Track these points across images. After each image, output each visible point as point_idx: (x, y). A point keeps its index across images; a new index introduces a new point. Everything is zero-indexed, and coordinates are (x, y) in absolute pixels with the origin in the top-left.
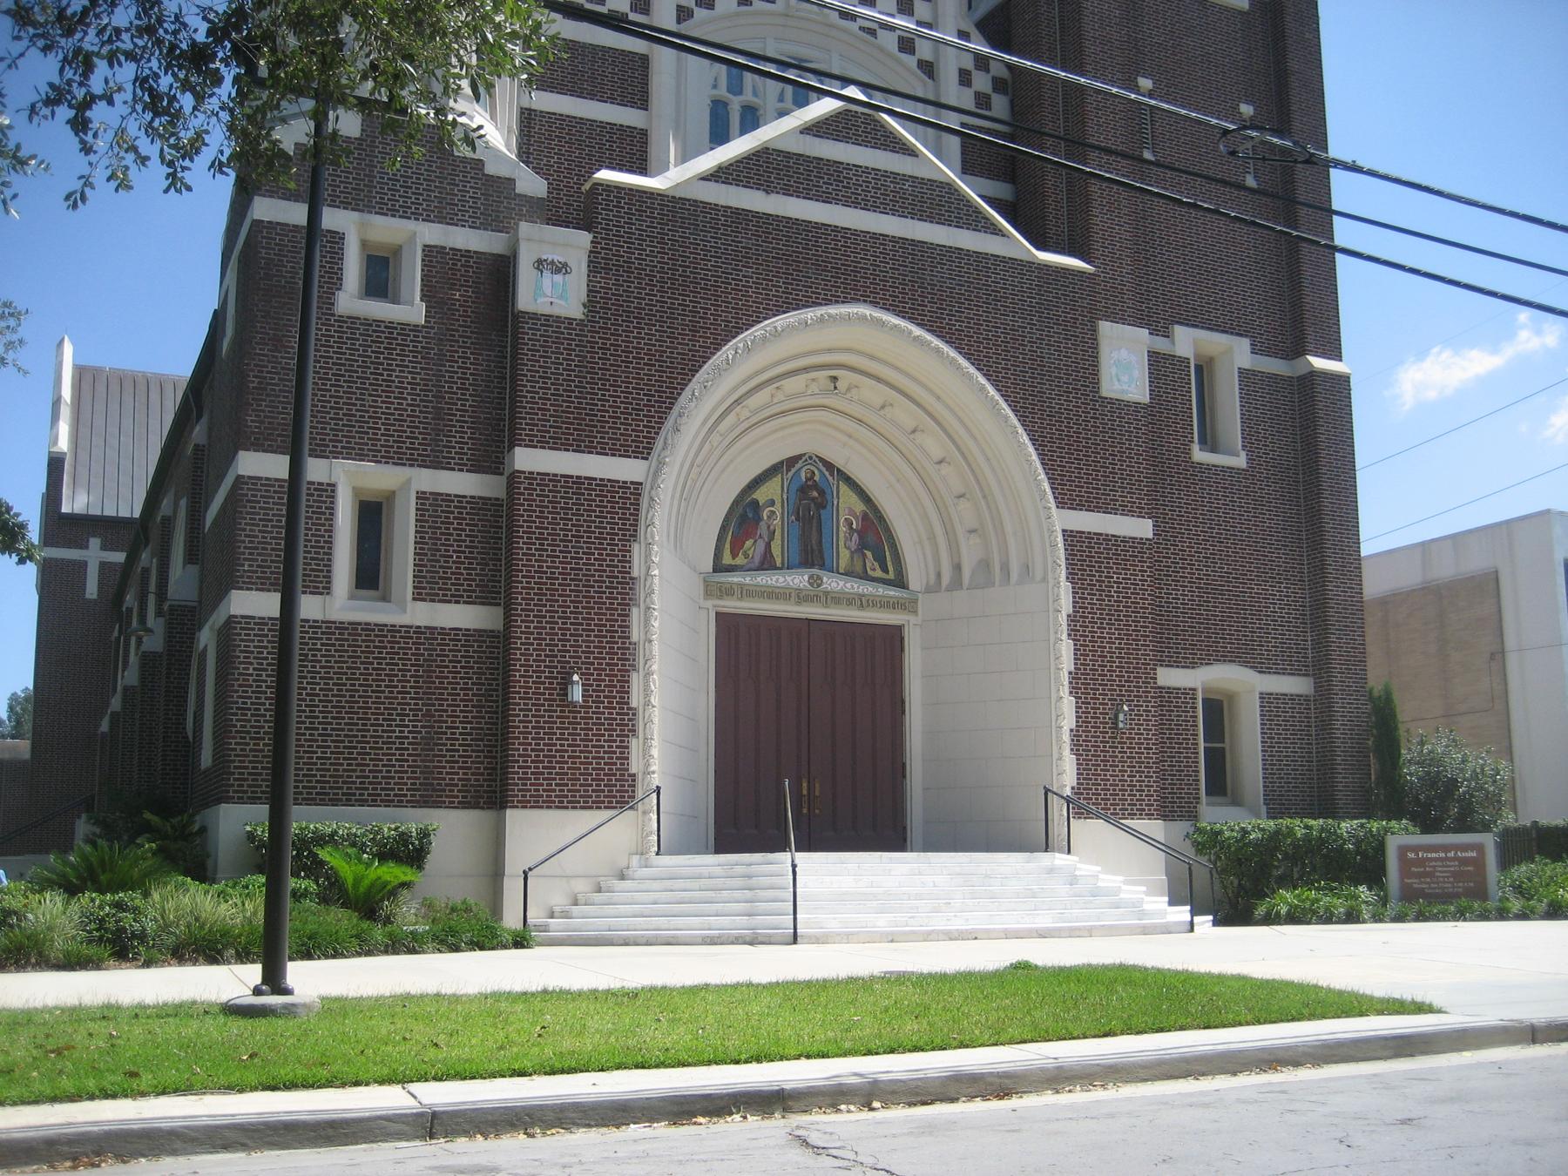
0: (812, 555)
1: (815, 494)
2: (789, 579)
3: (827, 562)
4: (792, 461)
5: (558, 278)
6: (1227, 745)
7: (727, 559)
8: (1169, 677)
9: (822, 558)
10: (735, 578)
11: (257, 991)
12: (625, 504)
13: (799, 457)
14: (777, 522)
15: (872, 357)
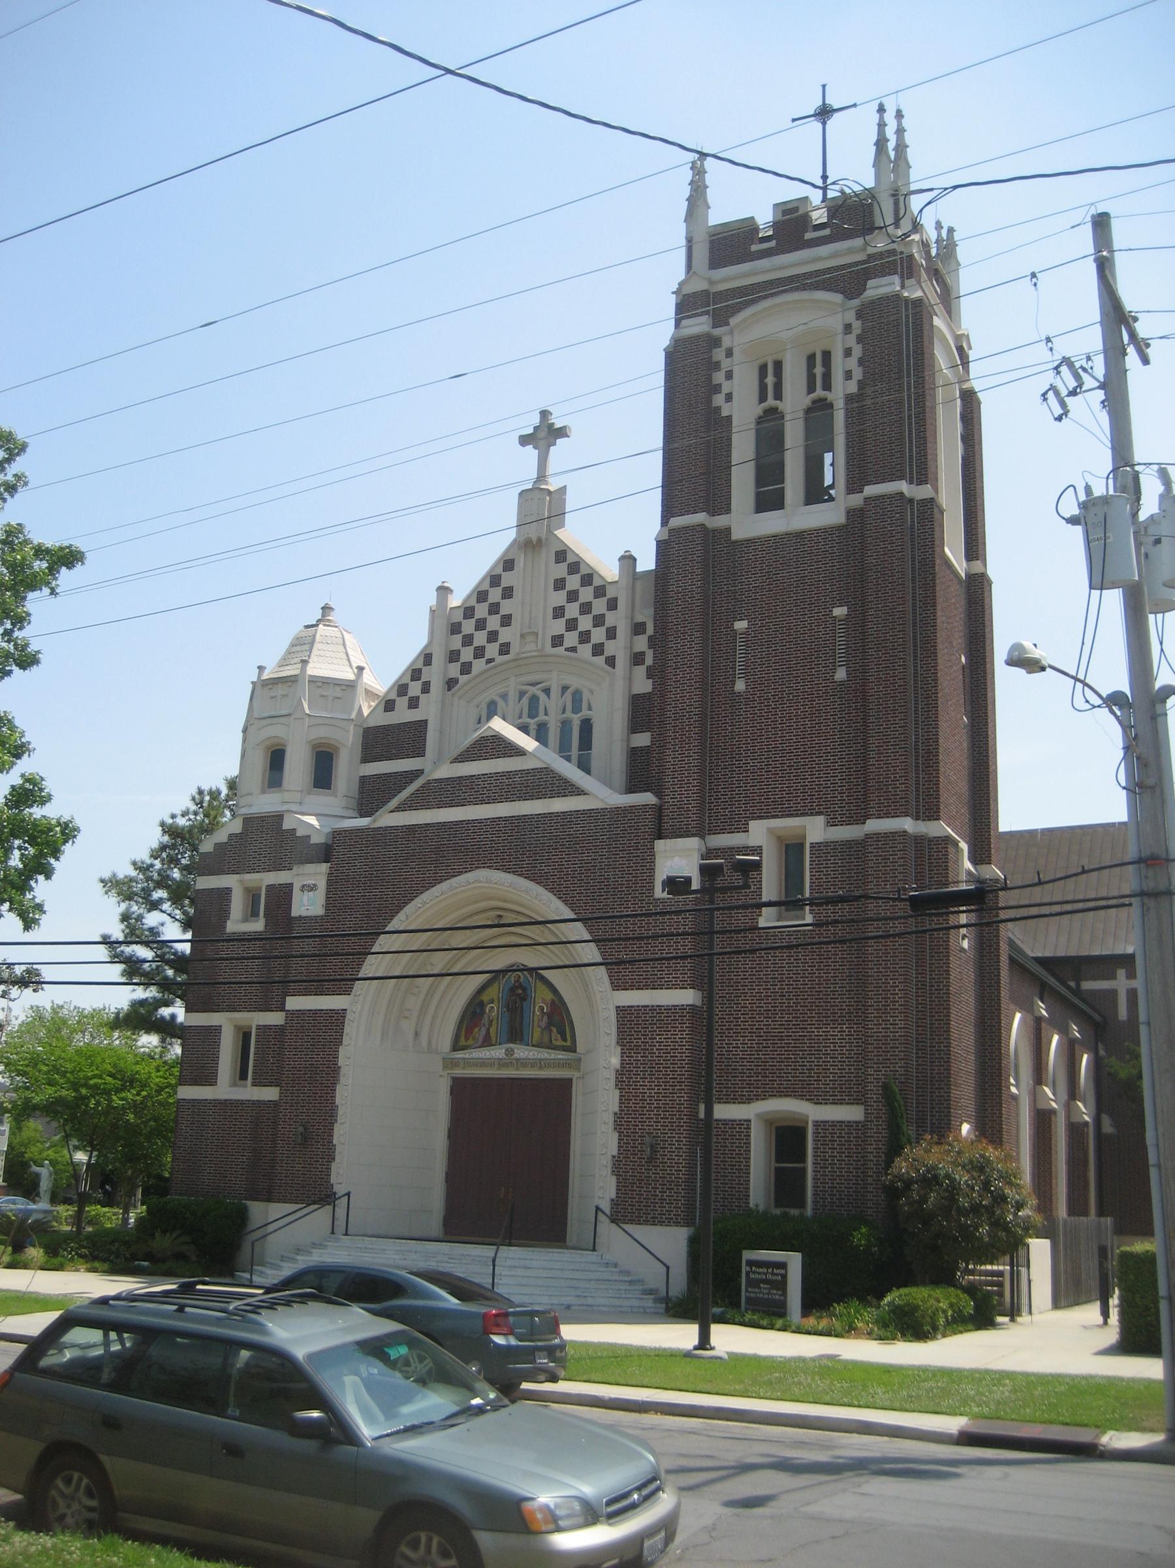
0: (516, 1034)
3: (525, 1037)
6: (774, 1165)
7: (463, 1042)
11: (696, 1348)
15: (505, 901)
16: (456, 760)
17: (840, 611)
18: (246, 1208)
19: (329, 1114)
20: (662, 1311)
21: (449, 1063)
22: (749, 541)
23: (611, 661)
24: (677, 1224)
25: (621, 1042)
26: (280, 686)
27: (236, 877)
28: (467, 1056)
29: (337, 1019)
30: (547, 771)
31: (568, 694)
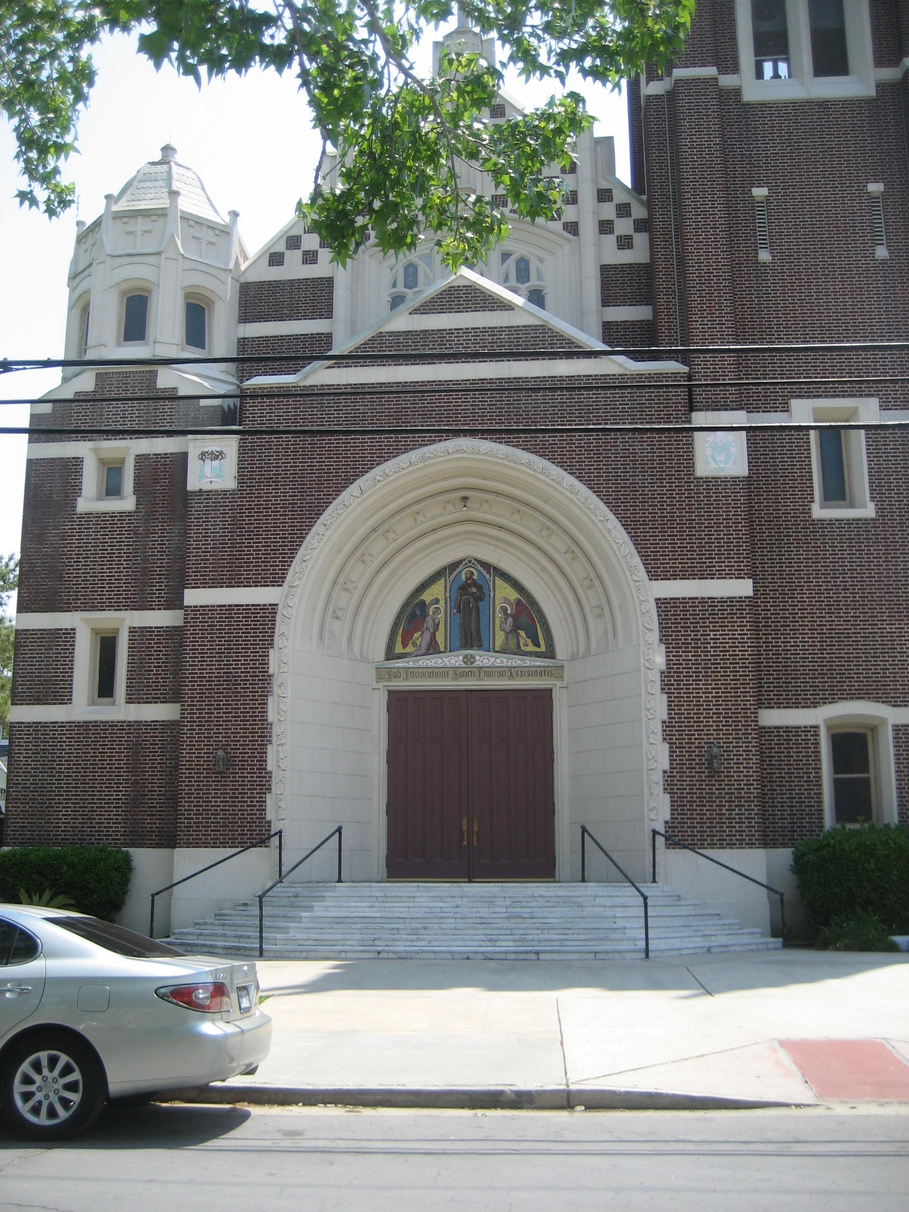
0: (471, 637)
1: (474, 590)
3: (485, 644)
4: (453, 566)
5: (216, 463)
6: (871, 775)
7: (399, 649)
8: (772, 717)
9: (480, 640)
10: (400, 663)
14: (441, 616)
15: (484, 478)
16: (415, 311)
17: (875, 188)
18: (127, 859)
19: (259, 734)
20: (780, 945)
21: (382, 674)
22: (763, 105)
23: (573, 228)
24: (751, 845)
25: (665, 638)
26: (140, 219)
27: (90, 444)
28: (411, 664)
29: (265, 616)
30: (544, 330)
31: (511, 261)
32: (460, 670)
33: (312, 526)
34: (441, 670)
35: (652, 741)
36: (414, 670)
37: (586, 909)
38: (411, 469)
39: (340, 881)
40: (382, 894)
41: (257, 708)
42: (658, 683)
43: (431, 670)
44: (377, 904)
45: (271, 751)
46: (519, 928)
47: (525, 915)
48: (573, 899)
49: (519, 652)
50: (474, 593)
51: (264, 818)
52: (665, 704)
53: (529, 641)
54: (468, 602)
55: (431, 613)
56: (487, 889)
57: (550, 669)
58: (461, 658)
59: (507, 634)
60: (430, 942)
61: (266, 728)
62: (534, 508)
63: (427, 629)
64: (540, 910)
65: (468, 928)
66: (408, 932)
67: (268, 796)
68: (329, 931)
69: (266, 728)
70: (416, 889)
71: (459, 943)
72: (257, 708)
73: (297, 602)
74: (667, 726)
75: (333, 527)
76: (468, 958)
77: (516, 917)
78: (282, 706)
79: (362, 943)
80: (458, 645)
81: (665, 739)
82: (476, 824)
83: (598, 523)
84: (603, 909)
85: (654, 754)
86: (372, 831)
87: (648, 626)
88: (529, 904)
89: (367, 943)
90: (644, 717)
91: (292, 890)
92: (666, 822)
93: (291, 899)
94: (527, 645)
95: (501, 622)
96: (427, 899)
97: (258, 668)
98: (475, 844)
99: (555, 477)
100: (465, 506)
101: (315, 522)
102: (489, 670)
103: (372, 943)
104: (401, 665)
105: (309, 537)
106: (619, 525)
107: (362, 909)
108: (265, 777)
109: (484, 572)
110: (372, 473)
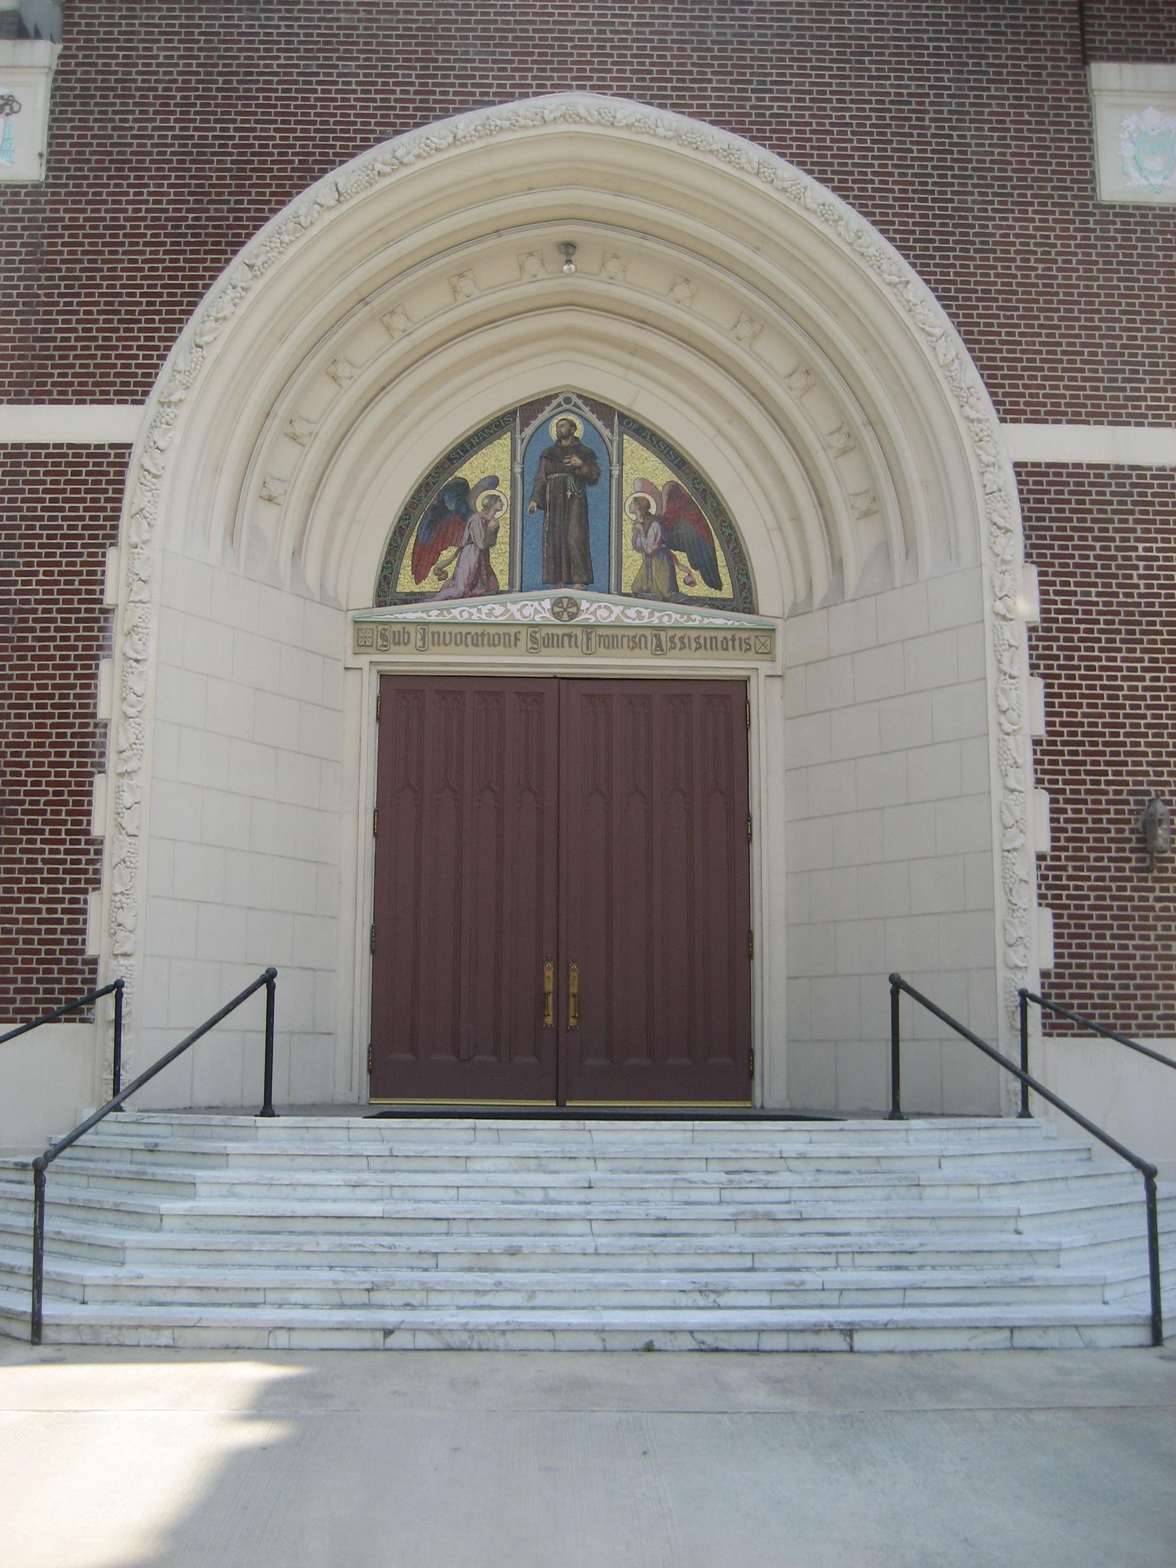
0: (569, 561)
1: (576, 461)
2: (513, 608)
4: (531, 409)
7: (406, 583)
10: (410, 613)
12: (92, 485)
13: (545, 401)
14: (502, 516)
21: (369, 637)
25: (1035, 552)
28: (434, 616)
32: (545, 631)
33: (221, 269)
34: (501, 630)
35: (1012, 784)
36: (442, 629)
37: (928, 1192)
38: (454, 152)
39: (267, 1110)
40: (382, 1149)
41: (73, 687)
42: (1024, 652)
43: (479, 630)
44: (366, 1177)
45: (102, 789)
46: (773, 1252)
47: (780, 1211)
48: (885, 1165)
49: (673, 595)
50: (575, 468)
51: (82, 952)
52: (1040, 700)
53: (696, 575)
54: (564, 486)
55: (479, 508)
56: (652, 1137)
57: (744, 635)
58: (547, 604)
59: (648, 557)
60: (532, 1294)
61: (93, 735)
62: (727, 264)
63: (470, 541)
64: (808, 1194)
65: (634, 1251)
66: (464, 1261)
67: (92, 897)
68: (240, 1258)
69: (93, 735)
70: (469, 1135)
71: (617, 1298)
72: (73, 687)
73: (177, 440)
74: (1047, 756)
75: (270, 273)
76: (649, 1348)
77: (756, 1217)
78: (131, 680)
79: (334, 1298)
80: (539, 579)
81: (1039, 781)
82: (574, 975)
83: (887, 292)
84: (971, 1192)
85: (1018, 814)
86: (336, 997)
87: (1001, 522)
88: (772, 1180)
89: (348, 1298)
90: (993, 730)
91: (144, 1130)
92: (1045, 974)
93: (139, 1157)
94: (692, 584)
95: (636, 533)
96: (503, 1164)
97: (78, 592)
98: (573, 1022)
99: (786, 184)
100: (569, 262)
101: (228, 261)
102: (610, 632)
103: (363, 1298)
104: (411, 616)
105: (210, 295)
106: (931, 296)
107: (328, 1192)
108: (87, 852)
109: (599, 424)
110: (365, 158)
